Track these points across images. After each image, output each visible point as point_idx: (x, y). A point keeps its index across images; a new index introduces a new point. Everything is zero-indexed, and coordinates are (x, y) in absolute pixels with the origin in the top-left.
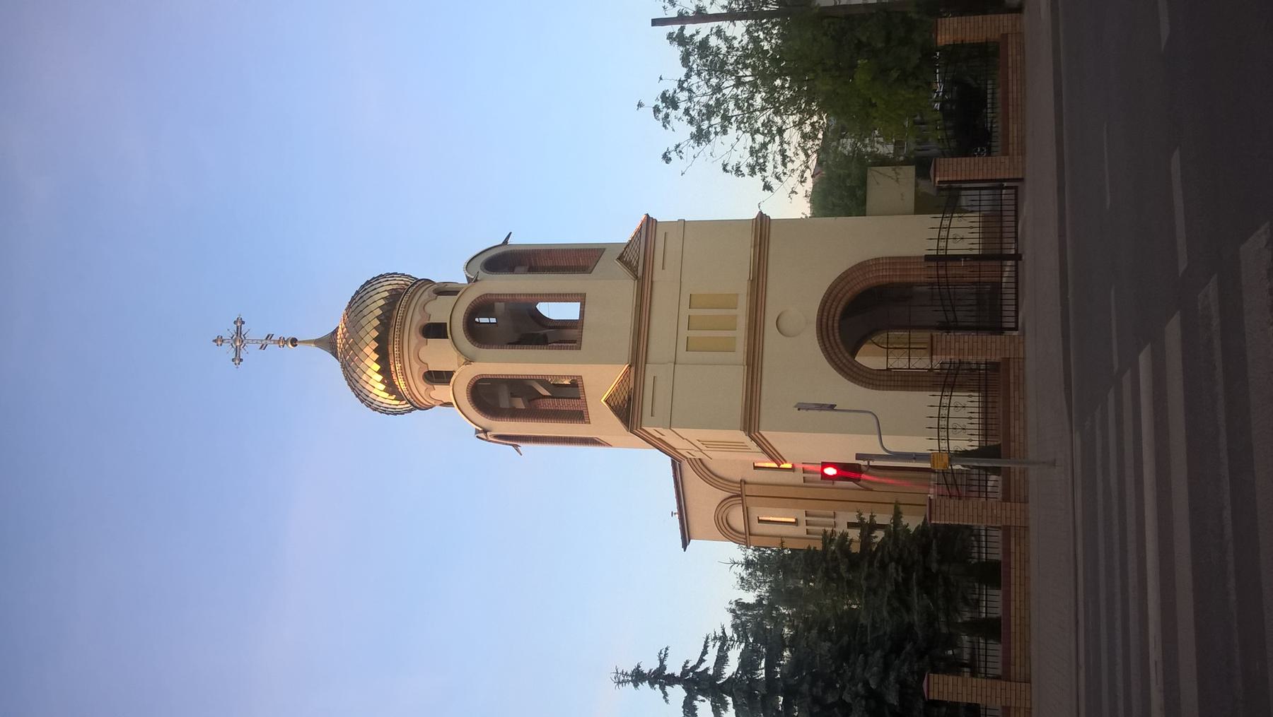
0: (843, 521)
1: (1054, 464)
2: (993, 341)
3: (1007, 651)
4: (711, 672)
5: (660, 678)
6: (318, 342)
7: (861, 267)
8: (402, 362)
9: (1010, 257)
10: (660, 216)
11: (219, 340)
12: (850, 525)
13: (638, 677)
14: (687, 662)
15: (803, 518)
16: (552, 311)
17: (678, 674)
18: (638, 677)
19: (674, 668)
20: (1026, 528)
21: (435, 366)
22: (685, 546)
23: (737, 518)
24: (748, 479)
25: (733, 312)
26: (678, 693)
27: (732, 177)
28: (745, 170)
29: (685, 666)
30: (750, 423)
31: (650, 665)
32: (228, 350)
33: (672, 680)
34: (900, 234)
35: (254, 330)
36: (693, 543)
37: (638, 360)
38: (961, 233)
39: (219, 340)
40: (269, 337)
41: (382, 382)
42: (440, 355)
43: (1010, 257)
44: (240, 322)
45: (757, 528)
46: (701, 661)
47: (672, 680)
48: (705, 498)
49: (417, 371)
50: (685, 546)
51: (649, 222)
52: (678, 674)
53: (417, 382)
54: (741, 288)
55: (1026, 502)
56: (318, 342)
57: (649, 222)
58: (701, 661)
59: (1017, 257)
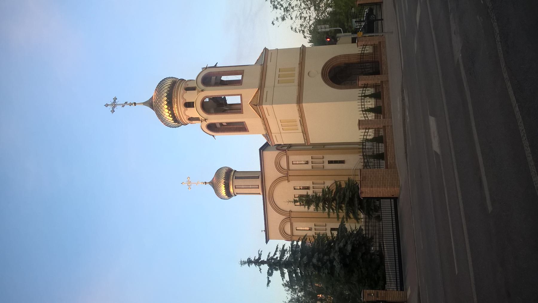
0: (329, 183)
1: (392, 32)
2: (378, 76)
3: (386, 163)
4: (279, 259)
5: (258, 262)
6: (144, 104)
7: (336, 58)
8: (177, 99)
9: (379, 20)
10: (271, 47)
11: (107, 105)
12: (332, 229)
13: (249, 262)
14: (270, 253)
15: (313, 227)
16: (230, 100)
17: (266, 260)
18: (249, 262)
19: (264, 258)
20: (388, 81)
21: (188, 100)
22: (267, 242)
23: (288, 230)
24: (293, 210)
25: (293, 78)
26: (265, 268)
27: (293, 32)
28: (298, 31)
29: (269, 256)
30: (299, 101)
31: (254, 256)
32: (110, 108)
33: (263, 262)
34: (346, 48)
35: (120, 101)
36: (270, 241)
37: (261, 87)
38: (370, 133)
39: (107, 105)
40: (126, 103)
41: (167, 109)
42: (190, 96)
43: (379, 20)
44: (115, 99)
45: (296, 233)
46: (275, 254)
47: (263, 262)
48: (276, 219)
49: (182, 102)
50: (267, 242)
51: (266, 49)
52: (266, 260)
53: (182, 107)
54: (297, 66)
55: (388, 74)
56: (144, 104)
57: (266, 49)
58: (275, 254)
59: (382, 20)
